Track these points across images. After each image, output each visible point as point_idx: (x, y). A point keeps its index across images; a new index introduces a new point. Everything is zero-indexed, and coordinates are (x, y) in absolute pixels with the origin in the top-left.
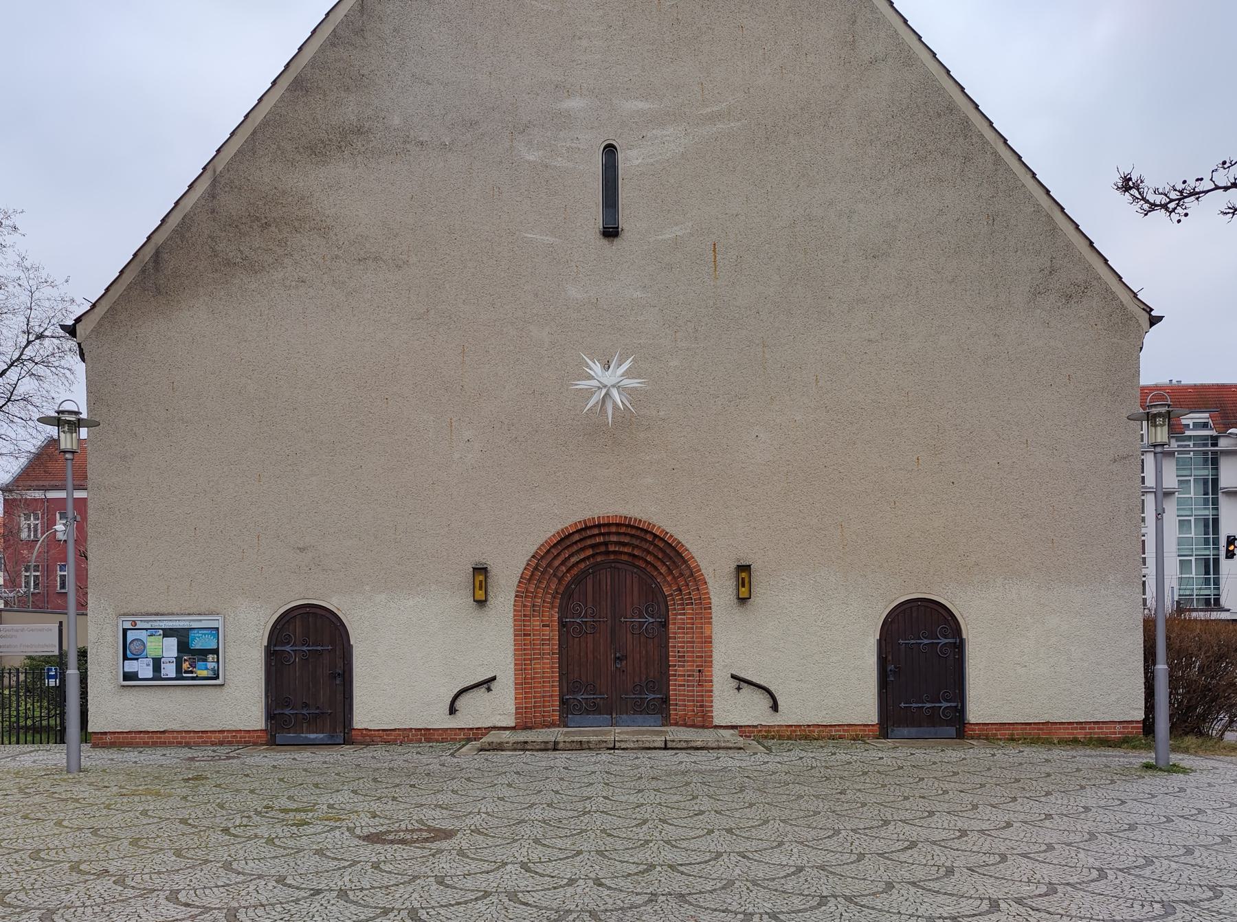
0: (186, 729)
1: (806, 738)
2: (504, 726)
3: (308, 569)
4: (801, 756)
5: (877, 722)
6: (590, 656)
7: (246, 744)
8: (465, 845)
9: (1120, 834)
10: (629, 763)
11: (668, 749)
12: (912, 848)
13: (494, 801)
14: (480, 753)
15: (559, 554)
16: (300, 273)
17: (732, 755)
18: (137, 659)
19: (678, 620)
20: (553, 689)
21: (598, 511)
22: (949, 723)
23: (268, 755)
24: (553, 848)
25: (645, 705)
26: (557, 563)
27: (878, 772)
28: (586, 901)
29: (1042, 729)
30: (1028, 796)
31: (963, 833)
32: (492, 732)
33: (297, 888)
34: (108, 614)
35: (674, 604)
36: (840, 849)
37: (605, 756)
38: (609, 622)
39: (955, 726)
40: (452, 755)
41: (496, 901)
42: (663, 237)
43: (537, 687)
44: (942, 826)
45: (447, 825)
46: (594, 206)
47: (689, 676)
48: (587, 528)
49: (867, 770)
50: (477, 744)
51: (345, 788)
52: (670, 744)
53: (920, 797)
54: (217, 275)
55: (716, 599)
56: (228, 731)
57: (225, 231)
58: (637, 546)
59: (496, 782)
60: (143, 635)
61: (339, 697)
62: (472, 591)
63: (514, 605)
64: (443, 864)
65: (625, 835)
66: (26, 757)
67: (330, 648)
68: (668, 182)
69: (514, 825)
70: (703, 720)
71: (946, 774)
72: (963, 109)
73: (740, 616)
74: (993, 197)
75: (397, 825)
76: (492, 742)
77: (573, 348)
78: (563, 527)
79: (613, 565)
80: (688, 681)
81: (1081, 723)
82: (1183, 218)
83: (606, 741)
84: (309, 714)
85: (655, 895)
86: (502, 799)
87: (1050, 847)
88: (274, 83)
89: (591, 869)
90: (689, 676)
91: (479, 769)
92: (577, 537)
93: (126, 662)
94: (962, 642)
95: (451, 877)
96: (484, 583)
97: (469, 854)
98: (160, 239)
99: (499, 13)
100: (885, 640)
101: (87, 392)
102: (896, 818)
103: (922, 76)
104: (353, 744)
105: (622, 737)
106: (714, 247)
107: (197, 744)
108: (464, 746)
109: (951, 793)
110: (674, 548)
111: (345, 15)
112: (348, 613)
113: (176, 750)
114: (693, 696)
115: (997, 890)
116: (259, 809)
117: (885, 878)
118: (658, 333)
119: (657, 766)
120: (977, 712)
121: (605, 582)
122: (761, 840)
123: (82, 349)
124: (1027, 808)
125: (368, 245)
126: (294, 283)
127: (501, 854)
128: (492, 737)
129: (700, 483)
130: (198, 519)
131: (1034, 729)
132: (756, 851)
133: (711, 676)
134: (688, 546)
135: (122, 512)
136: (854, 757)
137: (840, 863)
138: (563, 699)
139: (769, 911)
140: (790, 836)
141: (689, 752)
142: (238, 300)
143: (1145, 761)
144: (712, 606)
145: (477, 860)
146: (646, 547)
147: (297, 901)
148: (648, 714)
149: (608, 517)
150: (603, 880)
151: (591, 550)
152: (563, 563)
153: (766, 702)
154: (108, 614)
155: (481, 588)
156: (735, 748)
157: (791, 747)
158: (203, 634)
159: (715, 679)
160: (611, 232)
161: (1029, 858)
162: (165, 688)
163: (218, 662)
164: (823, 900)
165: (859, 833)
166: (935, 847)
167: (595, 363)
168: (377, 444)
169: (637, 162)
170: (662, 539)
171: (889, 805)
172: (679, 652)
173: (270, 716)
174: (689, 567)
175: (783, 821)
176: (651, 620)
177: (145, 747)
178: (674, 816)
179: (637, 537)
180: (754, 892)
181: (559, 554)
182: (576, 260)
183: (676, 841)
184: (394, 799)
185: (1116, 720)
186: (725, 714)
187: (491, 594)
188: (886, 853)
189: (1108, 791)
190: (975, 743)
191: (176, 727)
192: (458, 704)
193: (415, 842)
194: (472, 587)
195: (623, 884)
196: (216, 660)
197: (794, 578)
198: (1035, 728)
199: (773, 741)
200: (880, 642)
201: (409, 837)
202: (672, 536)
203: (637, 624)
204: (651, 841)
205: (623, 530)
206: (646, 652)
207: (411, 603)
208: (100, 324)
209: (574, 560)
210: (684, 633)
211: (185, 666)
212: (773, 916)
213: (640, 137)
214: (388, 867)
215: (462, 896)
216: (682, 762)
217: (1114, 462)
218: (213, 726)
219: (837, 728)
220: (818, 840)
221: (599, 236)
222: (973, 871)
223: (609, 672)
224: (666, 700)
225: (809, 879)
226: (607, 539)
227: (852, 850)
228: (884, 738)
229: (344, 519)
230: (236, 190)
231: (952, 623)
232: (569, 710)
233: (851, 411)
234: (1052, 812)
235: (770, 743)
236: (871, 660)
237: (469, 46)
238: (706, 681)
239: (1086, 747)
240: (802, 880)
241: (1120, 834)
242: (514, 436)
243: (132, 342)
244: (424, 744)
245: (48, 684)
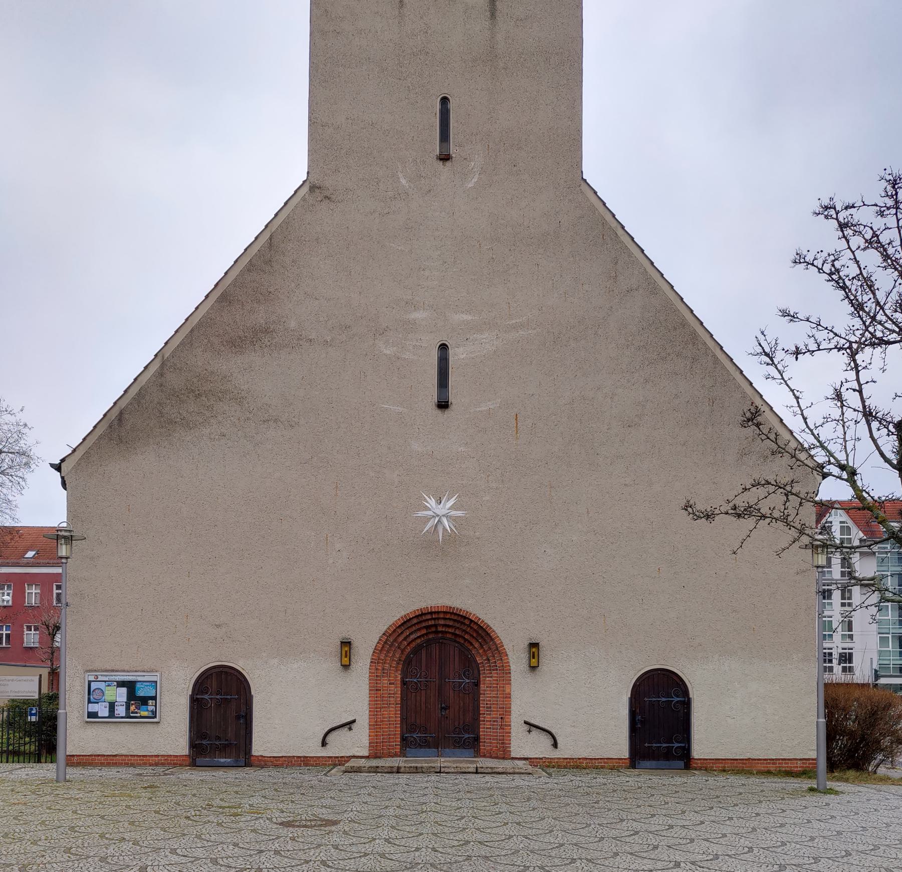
0: (132, 754)
2: (361, 755)
3: (222, 640)
4: (572, 779)
5: (628, 757)
6: (423, 707)
7: (175, 765)
8: (347, 829)
9: (772, 829)
10: (451, 782)
11: (479, 773)
12: (635, 835)
13: (360, 804)
14: (345, 774)
15: (402, 633)
16: (221, 430)
17: (523, 778)
18: (98, 703)
19: (487, 681)
20: (395, 730)
22: (679, 758)
23: (193, 773)
24: (404, 831)
25: (462, 742)
26: (401, 639)
27: (624, 790)
28: (428, 859)
29: (745, 764)
30: (721, 806)
31: (671, 827)
32: (352, 760)
33: (248, 849)
34: (78, 670)
36: (589, 835)
37: (433, 777)
38: (437, 682)
39: (683, 760)
40: (325, 775)
41: (373, 858)
42: (480, 409)
43: (385, 728)
44: (657, 823)
45: (331, 817)
46: (432, 387)
47: (494, 721)
48: (423, 614)
49: (616, 789)
50: (343, 768)
51: (257, 794)
52: (480, 770)
53: (648, 806)
54: (163, 430)
57: (169, 399)
58: (458, 628)
59: (359, 792)
60: (102, 686)
61: (243, 732)
62: (340, 658)
63: (370, 669)
64: (335, 839)
65: (450, 825)
66: (19, 772)
67: (237, 697)
68: (484, 370)
69: (376, 818)
70: (504, 754)
71: (670, 792)
72: (692, 324)
73: (531, 679)
74: (713, 386)
75: (299, 817)
76: (354, 767)
77: (415, 486)
78: (405, 613)
80: (493, 725)
81: (773, 760)
82: (712, 522)
83: (434, 767)
84: (220, 744)
85: (470, 857)
86: (366, 803)
87: (724, 835)
88: (207, 297)
89: (429, 843)
90: (494, 721)
91: (346, 784)
92: (415, 621)
93: (89, 704)
94: (689, 700)
95: (342, 845)
96: (348, 652)
97: (350, 833)
98: (123, 404)
99: (367, 251)
100: (635, 698)
101: (68, 512)
102: (629, 818)
103: (663, 302)
104: (251, 767)
105: (446, 764)
106: (516, 417)
107: (140, 765)
108: (332, 769)
109: (670, 804)
110: (484, 630)
111: (259, 250)
112: (250, 672)
113: (125, 769)
114: (497, 736)
115: (682, 857)
116: (204, 806)
117: (614, 850)
118: (476, 477)
119: (471, 784)
120: (698, 751)
122: (539, 829)
123: (65, 481)
124: (717, 814)
125: (270, 411)
126: (217, 437)
127: (371, 834)
128: (352, 763)
130: (144, 603)
131: (740, 763)
132: (535, 835)
133: (510, 722)
134: (495, 628)
135: (90, 597)
136: (609, 781)
137: (587, 842)
138: (403, 737)
139: (539, 865)
140: (558, 827)
141: (493, 775)
142: (177, 448)
143: (809, 786)
145: (356, 837)
146: (464, 629)
147: (251, 856)
149: (438, 607)
150: (437, 849)
151: (425, 630)
152: (405, 639)
153: (548, 741)
155: (346, 656)
156: (526, 773)
157: (566, 773)
158: (145, 685)
159: (512, 724)
160: (443, 405)
161: (708, 841)
162: (117, 724)
163: (156, 706)
164: (573, 861)
165: (603, 826)
166: (650, 834)
167: (430, 499)
168: (274, 552)
169: (462, 357)
170: (476, 623)
171: (626, 810)
172: (487, 704)
173: (193, 745)
174: (495, 644)
175: (554, 819)
176: (468, 681)
177: (102, 766)
178: (482, 814)
179: (458, 622)
180: (531, 856)
181: (402, 633)
182: (418, 424)
183: (483, 828)
184: (292, 802)
185: (798, 758)
186: (520, 749)
187: (353, 660)
188: (618, 837)
189: (777, 805)
190: (697, 773)
191: (124, 752)
192: (328, 739)
193: (314, 827)
194: (340, 655)
195: (450, 851)
196: (154, 704)
197: (570, 653)
198: (740, 763)
199: (553, 769)
200: (631, 699)
201: (309, 824)
202: (483, 621)
204: (467, 829)
205: (448, 616)
206: (464, 704)
207: (295, 666)
208: (78, 464)
209: (413, 637)
210: (491, 691)
211: (132, 708)
212: (542, 868)
213: (465, 339)
214: (301, 840)
215: (351, 855)
216: (488, 782)
217: (797, 574)
218: (150, 752)
219: (600, 761)
220: (575, 830)
221: (434, 407)
222: (670, 847)
223: (437, 719)
224: (477, 739)
225: (566, 850)
227: (596, 835)
228: (633, 768)
229: (249, 605)
230: (178, 371)
231: (682, 686)
232: (407, 744)
233: (612, 535)
234: (733, 816)
235: (552, 770)
236: (624, 712)
237: (346, 273)
238: (506, 725)
239: (776, 777)
240: (562, 850)
241: (772, 829)
242: (372, 548)
243: (100, 476)
244: (303, 768)
245: (31, 720)
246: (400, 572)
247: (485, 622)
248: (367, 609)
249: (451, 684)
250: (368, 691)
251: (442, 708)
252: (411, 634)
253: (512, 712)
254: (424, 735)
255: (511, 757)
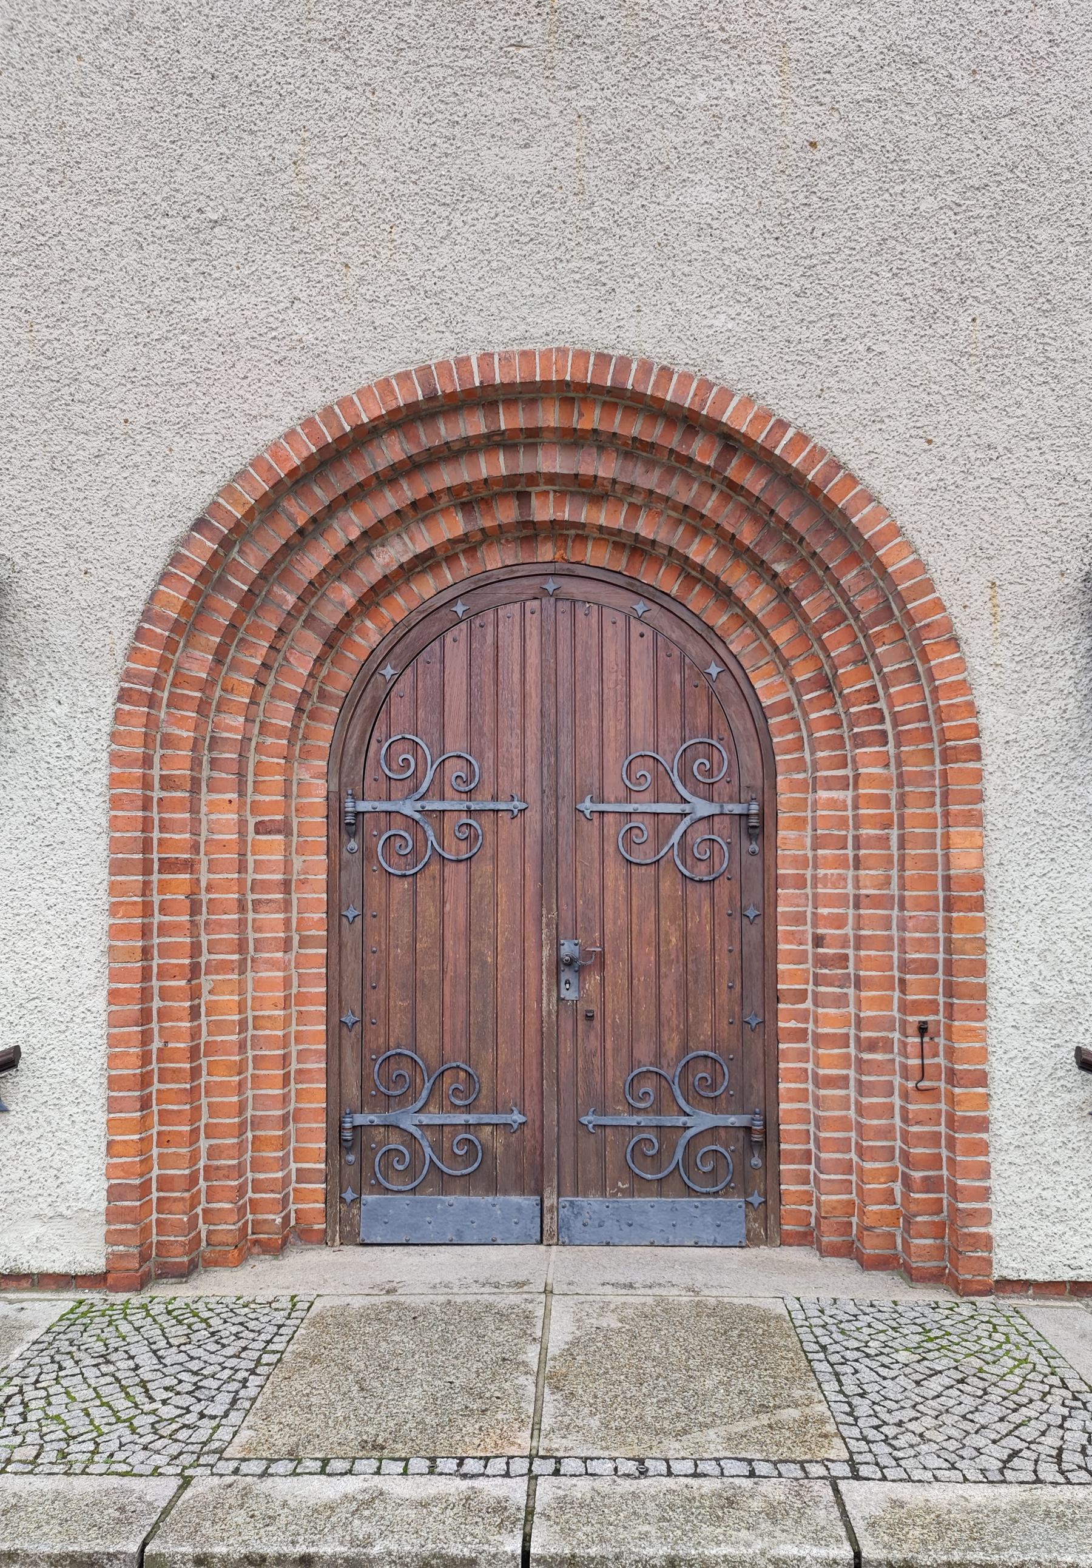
2: (59, 1268)
21: (482, 331)
25: (679, 1155)
35: (798, 744)
55: (1001, 710)
63: (114, 736)
78: (330, 398)
79: (550, 586)
121: (516, 676)
129: (927, 204)
134: (873, 479)
138: (341, 1129)
144: (984, 741)
148: (690, 1192)
176: (703, 808)
202: (802, 438)
203: (646, 825)
205: (592, 419)
206: (685, 936)
223: (532, 1018)
226: (524, 464)
246: (294, 148)
247: (818, 440)
248: (96, 375)
249: (609, 831)
250: (103, 874)
251: (562, 964)
252: (374, 535)
253: (993, 992)
254: (460, 1118)
255: (996, 1276)
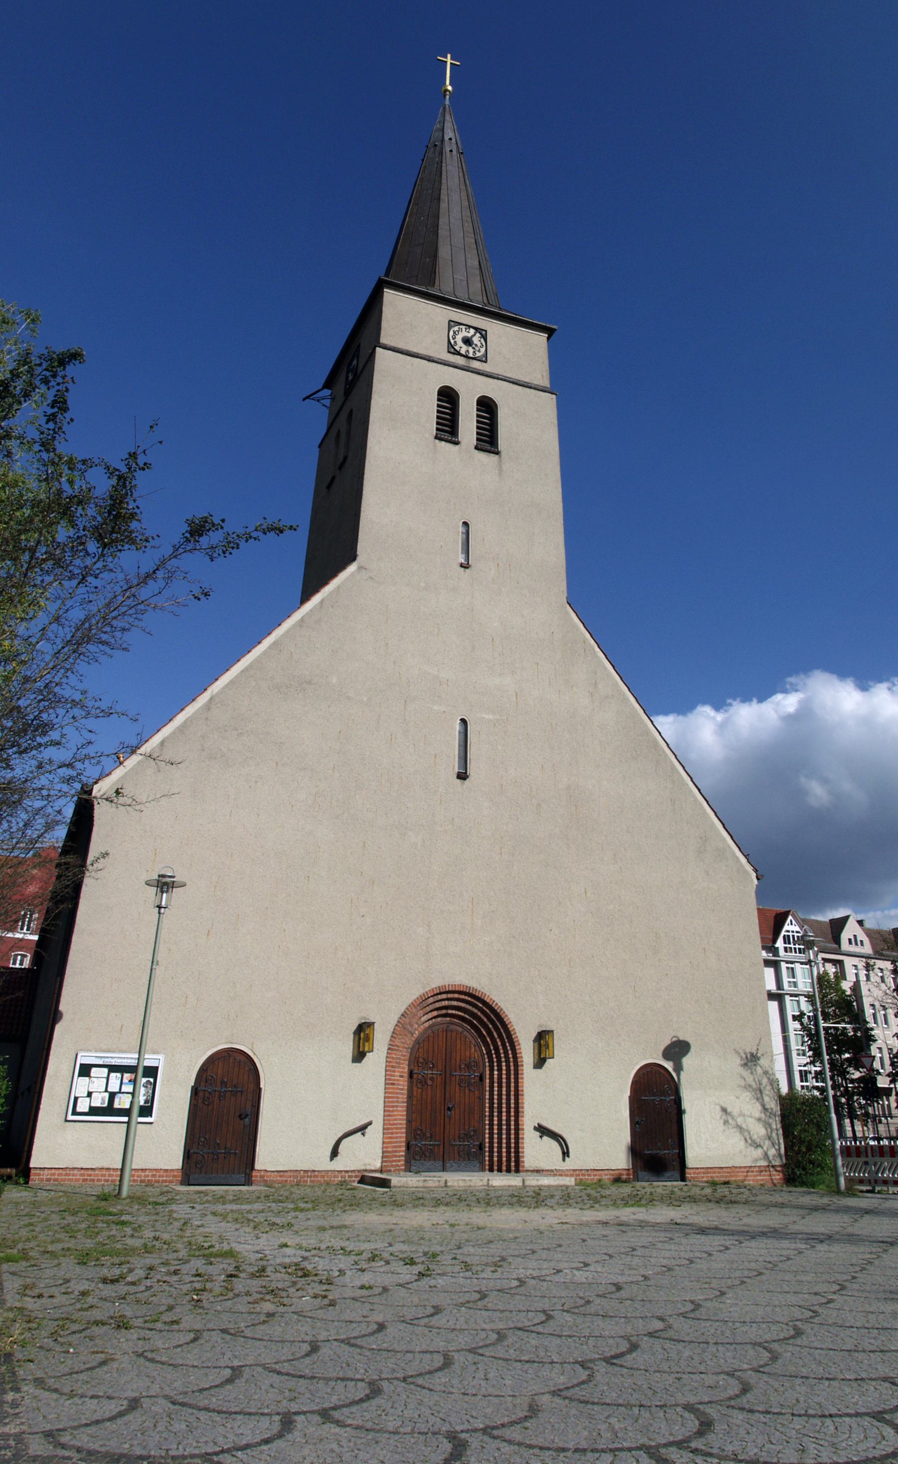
1: (824, 1209)
56: (150, 1170)
92: (431, 1000)
154: (69, 1049)
160: (462, 776)
